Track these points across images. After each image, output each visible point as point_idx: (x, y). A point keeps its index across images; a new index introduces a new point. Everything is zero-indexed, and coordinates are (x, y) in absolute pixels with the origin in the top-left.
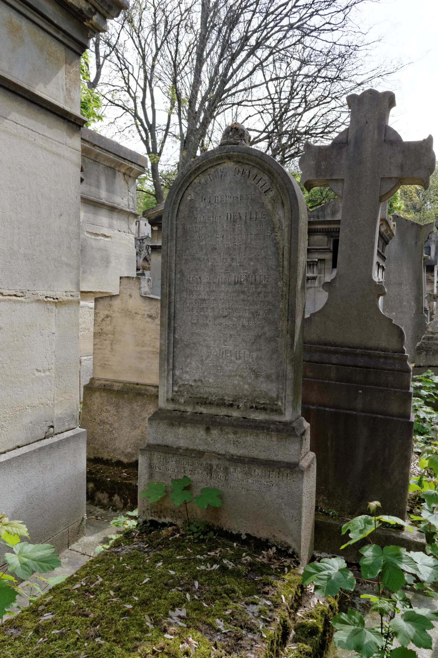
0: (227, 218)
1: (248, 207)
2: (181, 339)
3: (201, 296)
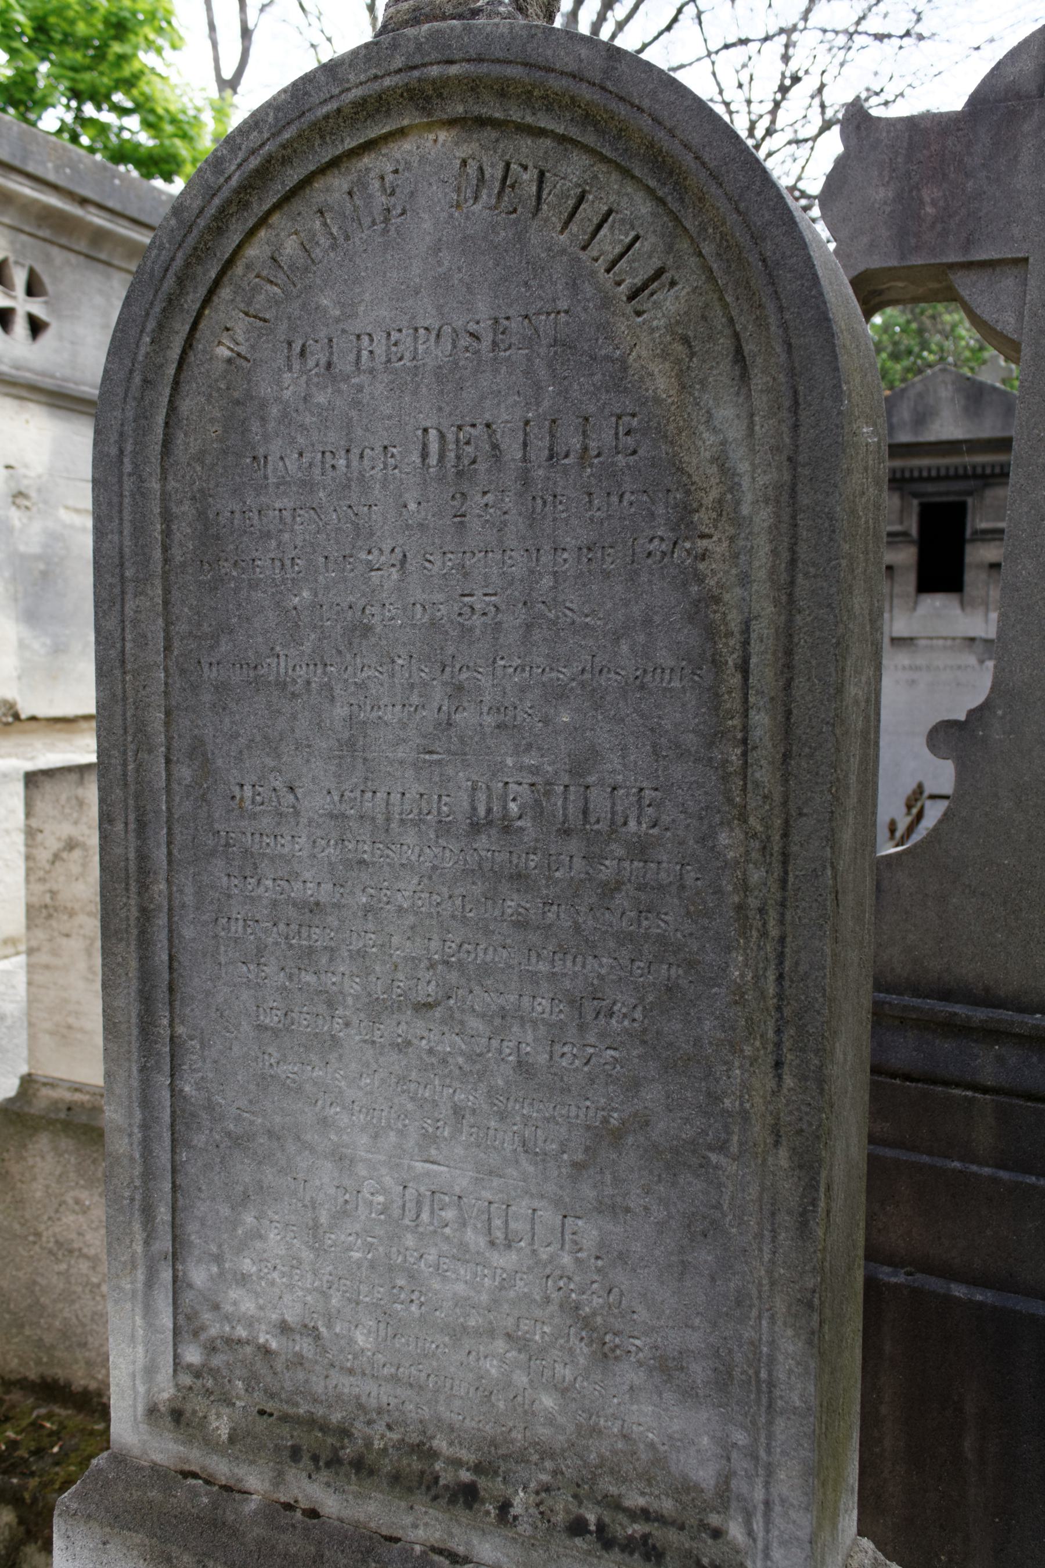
0: (424, 455)
1: (538, 388)
2: (210, 1107)
3: (298, 885)
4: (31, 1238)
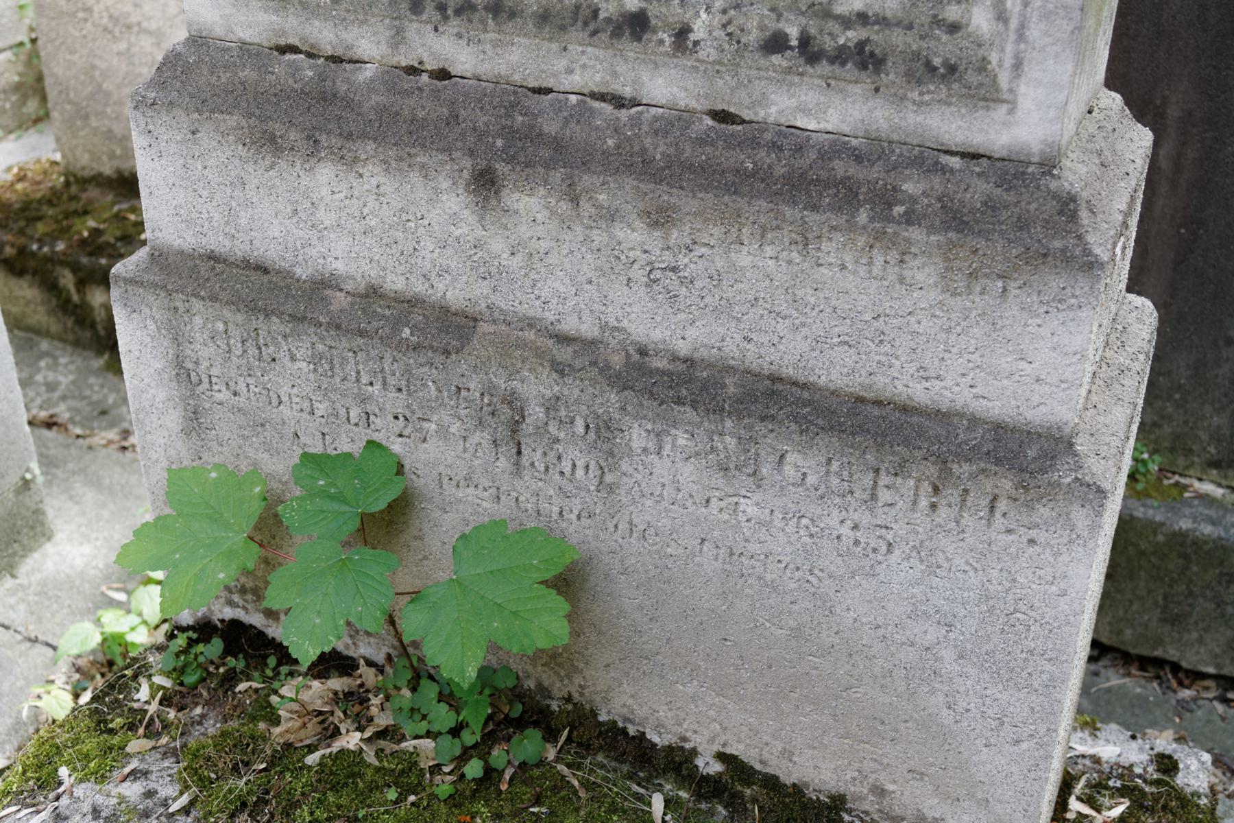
4: (80, 15)
